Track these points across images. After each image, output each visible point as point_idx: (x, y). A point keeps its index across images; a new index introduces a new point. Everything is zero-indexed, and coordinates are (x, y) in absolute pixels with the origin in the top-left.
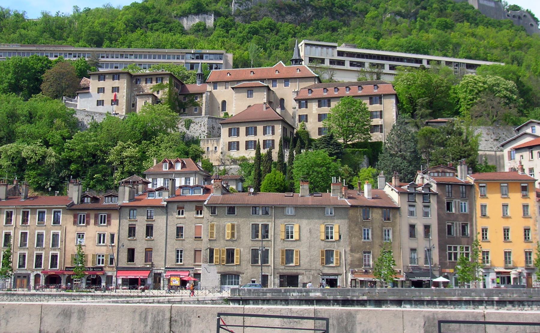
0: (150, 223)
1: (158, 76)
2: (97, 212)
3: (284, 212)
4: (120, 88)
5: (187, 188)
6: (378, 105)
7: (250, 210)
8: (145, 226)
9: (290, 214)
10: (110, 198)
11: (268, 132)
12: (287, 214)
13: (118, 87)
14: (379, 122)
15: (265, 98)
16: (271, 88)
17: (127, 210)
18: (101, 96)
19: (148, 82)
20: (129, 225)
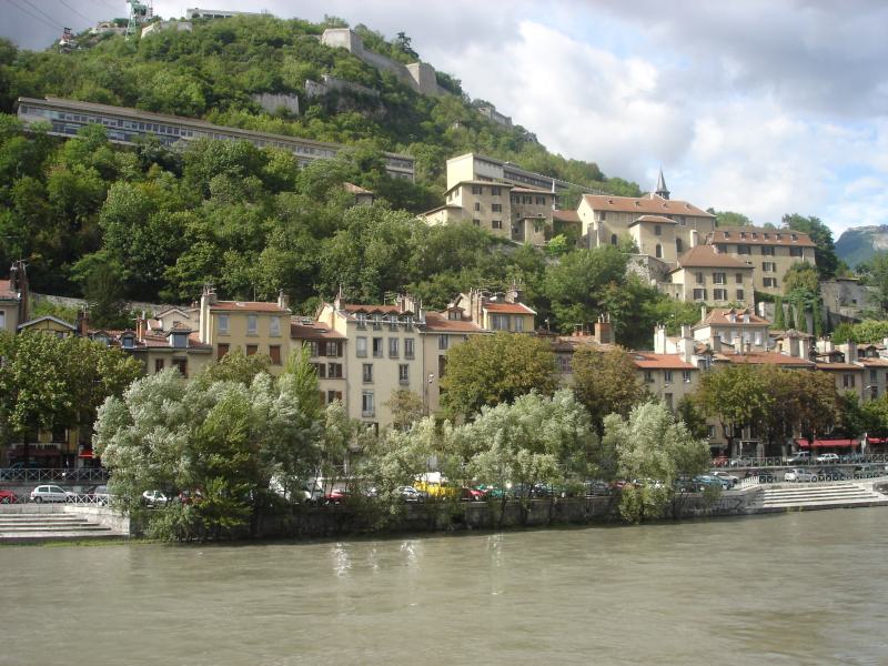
18: (497, 217)
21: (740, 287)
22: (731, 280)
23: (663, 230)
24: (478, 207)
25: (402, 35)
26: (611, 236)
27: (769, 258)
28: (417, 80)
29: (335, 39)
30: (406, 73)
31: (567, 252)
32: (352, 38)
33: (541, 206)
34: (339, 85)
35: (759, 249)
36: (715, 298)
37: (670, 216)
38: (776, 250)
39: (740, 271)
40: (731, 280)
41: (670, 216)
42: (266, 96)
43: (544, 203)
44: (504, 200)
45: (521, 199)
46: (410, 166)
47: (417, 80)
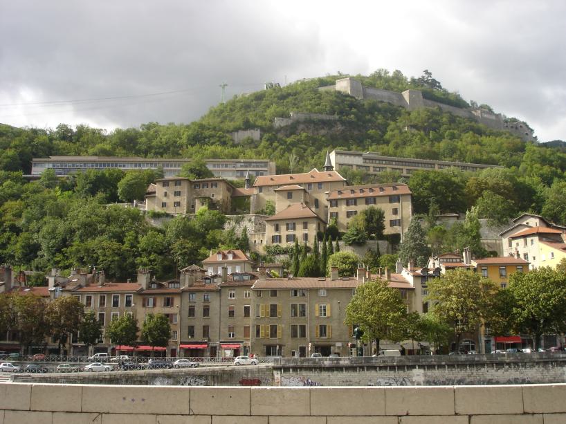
0: (206, 304)
17: (188, 294)
18: (178, 199)
21: (306, 231)
22: (299, 227)
23: (293, 195)
24: (166, 194)
25: (426, 72)
26: (313, 200)
27: (396, 205)
28: (408, 102)
29: (343, 86)
30: (402, 98)
31: (38, 220)
32: (351, 83)
33: (214, 188)
34: (302, 117)
35: (364, 201)
36: (287, 241)
37: (300, 184)
38: (377, 199)
39: (306, 221)
40: (299, 227)
41: (300, 184)
42: (241, 133)
43: (216, 186)
44: (184, 188)
45: (201, 185)
46: (266, 166)
47: (408, 102)
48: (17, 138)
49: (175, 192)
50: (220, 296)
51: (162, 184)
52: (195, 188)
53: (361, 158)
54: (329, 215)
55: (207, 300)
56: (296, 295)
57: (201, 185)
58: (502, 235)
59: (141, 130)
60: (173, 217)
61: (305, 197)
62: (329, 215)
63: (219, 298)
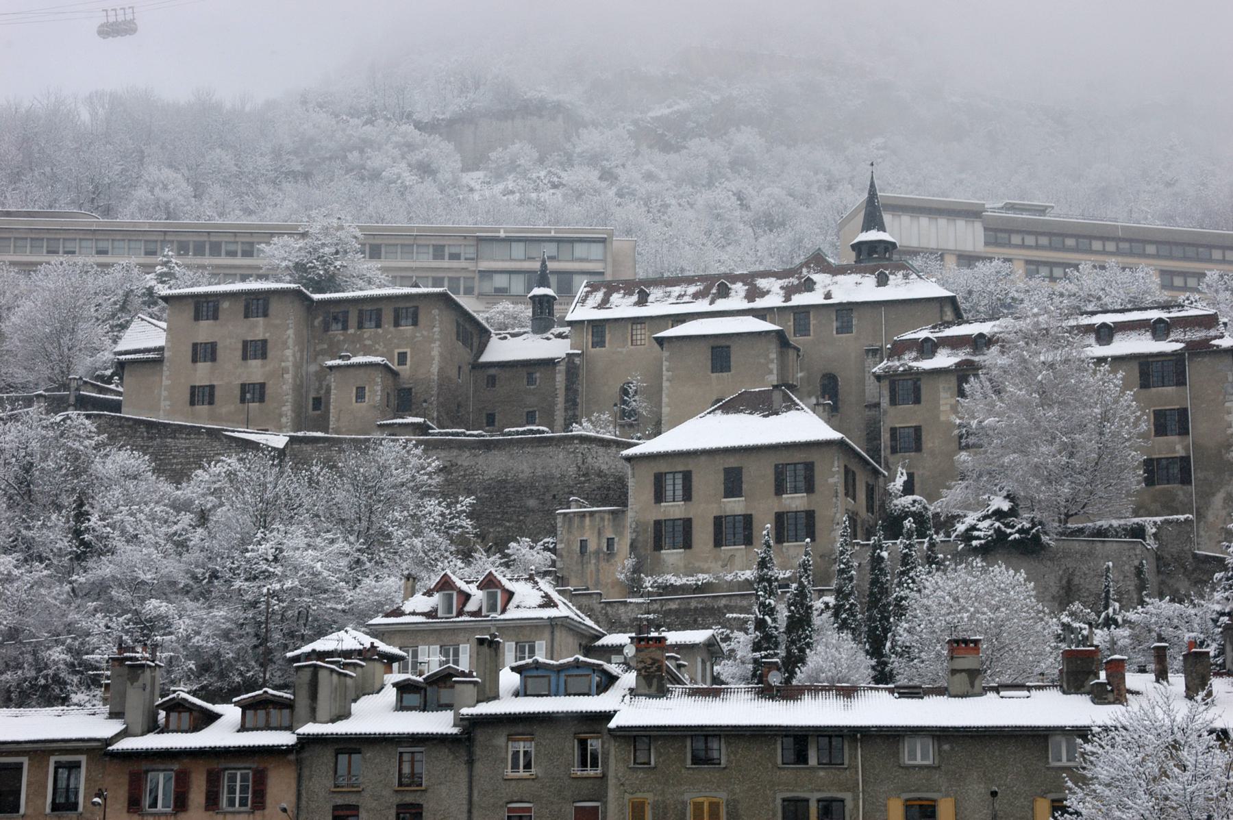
0: (409, 799)
1: (401, 305)
2: (215, 765)
3: (896, 754)
4: (269, 345)
5: (540, 673)
6: (1170, 389)
7: (775, 750)
8: (393, 812)
9: (919, 761)
10: (261, 713)
11: (669, 493)
12: (908, 762)
13: (265, 342)
14: (1178, 447)
15: (771, 372)
16: (793, 340)
17: (329, 753)
18: (255, 371)
19: (367, 324)
20: (907, 800)
33: (407, 329)
43: (415, 323)
48: (886, 393)
49: (245, 344)
50: (471, 763)
51: (190, 312)
52: (326, 328)
53: (978, 227)
54: (885, 437)
55: (410, 781)
56: (802, 758)
57: (353, 320)
58: (388, 394)
59: (85, 116)
60: (846, 466)
61: (783, 368)
62: (885, 437)
63: (463, 775)
